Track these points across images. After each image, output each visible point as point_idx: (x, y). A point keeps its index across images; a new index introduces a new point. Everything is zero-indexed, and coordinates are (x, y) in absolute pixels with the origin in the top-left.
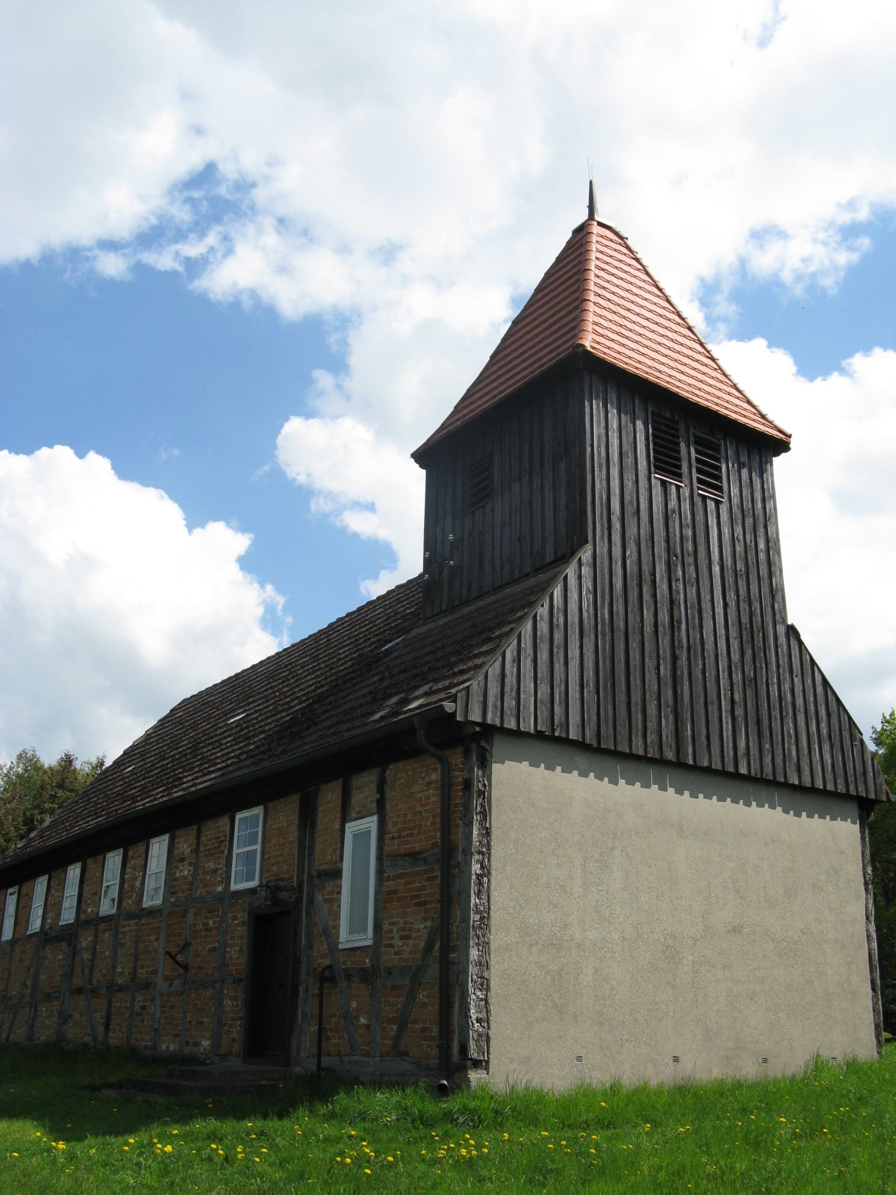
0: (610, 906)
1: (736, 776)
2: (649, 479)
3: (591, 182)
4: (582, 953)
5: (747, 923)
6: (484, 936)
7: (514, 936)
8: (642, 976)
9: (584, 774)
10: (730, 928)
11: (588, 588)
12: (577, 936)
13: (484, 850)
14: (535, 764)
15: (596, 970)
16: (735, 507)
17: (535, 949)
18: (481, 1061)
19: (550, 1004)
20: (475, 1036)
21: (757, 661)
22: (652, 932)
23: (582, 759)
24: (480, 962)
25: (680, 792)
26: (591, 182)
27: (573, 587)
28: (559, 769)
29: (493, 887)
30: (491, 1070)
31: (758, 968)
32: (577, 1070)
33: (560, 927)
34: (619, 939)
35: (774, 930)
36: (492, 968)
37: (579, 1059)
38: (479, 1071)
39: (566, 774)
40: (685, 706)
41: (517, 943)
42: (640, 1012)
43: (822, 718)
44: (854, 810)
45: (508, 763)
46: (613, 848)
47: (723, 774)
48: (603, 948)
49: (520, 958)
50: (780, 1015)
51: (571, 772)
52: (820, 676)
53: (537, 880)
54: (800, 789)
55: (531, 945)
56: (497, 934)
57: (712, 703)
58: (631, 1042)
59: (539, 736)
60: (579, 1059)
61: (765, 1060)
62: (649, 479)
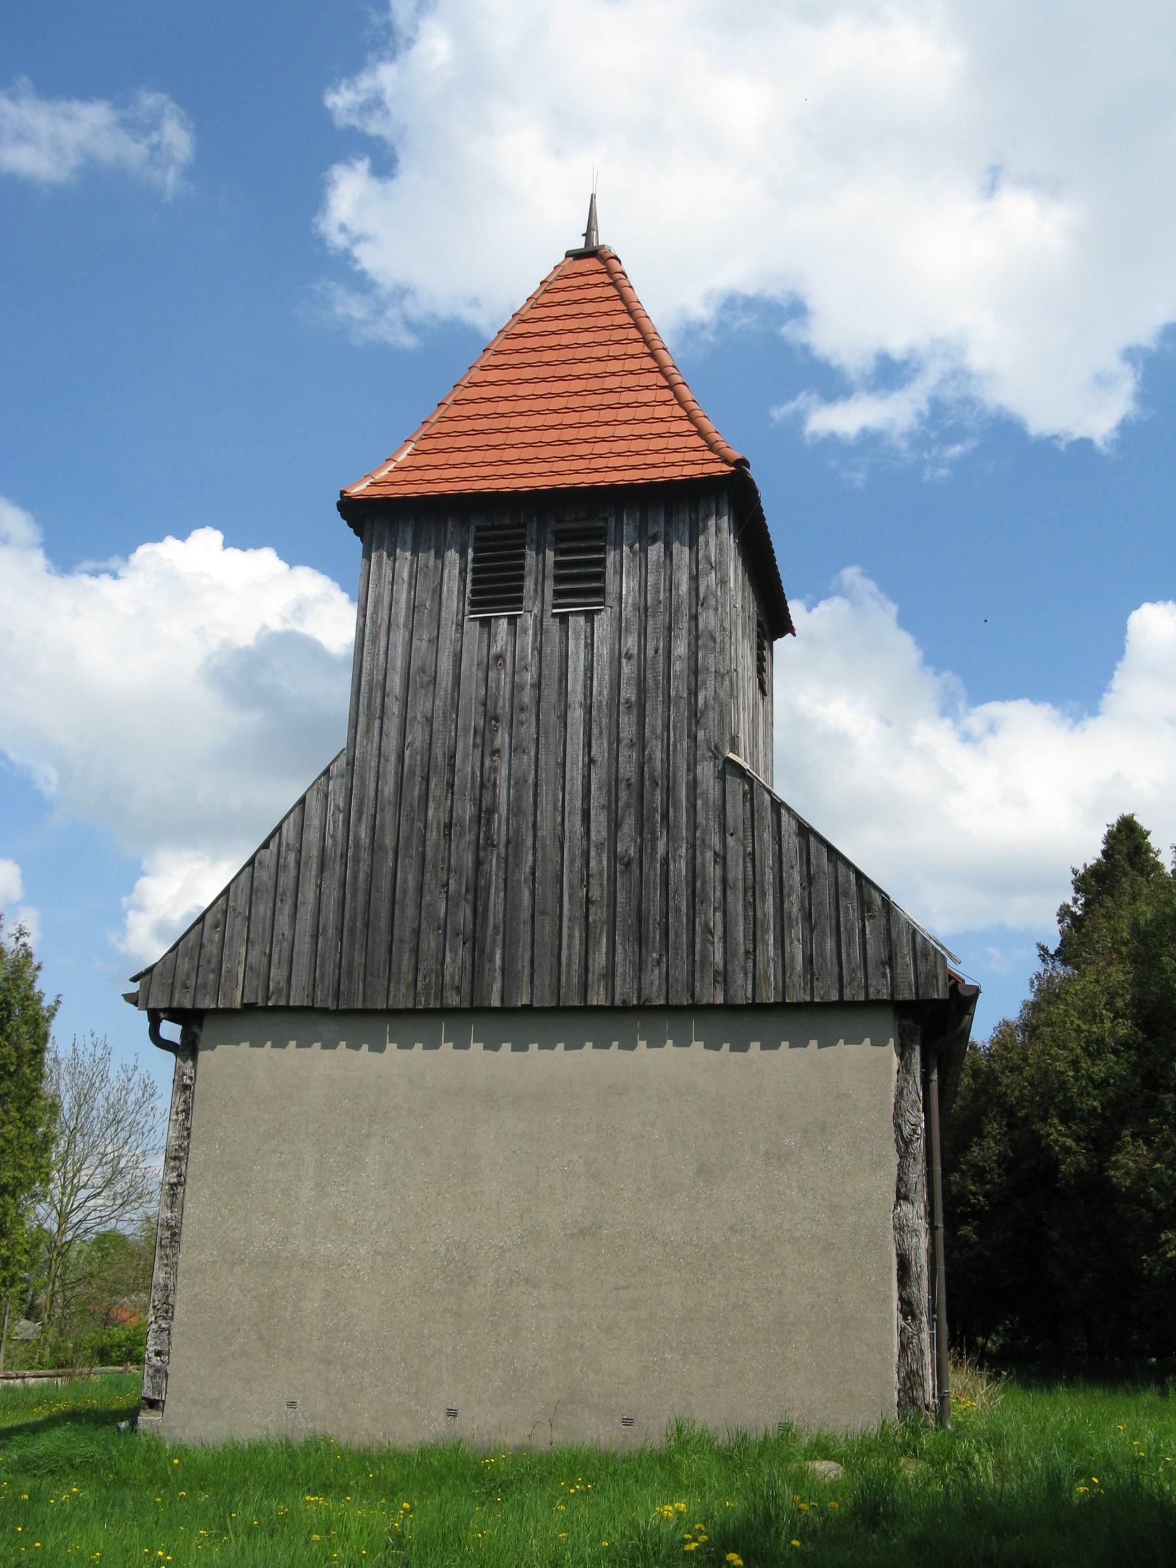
0: (357, 1211)
1: (587, 1010)
2: (460, 625)
3: (593, 197)
4: (306, 1273)
5: (610, 1221)
6: (174, 1255)
7: (211, 1254)
8: (402, 1302)
9: (329, 1045)
10: (575, 1231)
11: (337, 807)
12: (303, 1251)
13: (182, 1154)
14: (257, 1043)
15: (328, 1294)
16: (630, 608)
17: (237, 1269)
18: (158, 1401)
19: (253, 1336)
20: (151, 1371)
21: (646, 830)
22: (424, 1242)
23: (328, 1027)
24: (166, 1286)
25: (492, 1045)
26: (593, 197)
27: (313, 812)
28: (293, 1044)
29: (187, 1197)
30: (166, 1412)
31: (627, 1287)
32: (287, 1419)
33: (278, 1242)
34: (368, 1253)
35: (669, 1229)
36: (178, 1292)
37: (292, 1404)
38: (154, 1412)
39: (302, 1050)
40: (771, 892)
41: (215, 1262)
42: (394, 1349)
43: (791, 888)
44: (887, 1022)
45: (220, 1048)
46: (369, 1135)
47: (560, 1010)
48: (341, 1266)
49: (216, 1280)
50: (668, 1356)
51: (310, 1046)
52: (793, 822)
53: (248, 1184)
54: (730, 1009)
55: (233, 1265)
56: (187, 1253)
57: (543, 913)
58: (377, 1386)
59: (249, 1009)
60: (292, 1404)
61: (628, 1422)
62: (460, 625)
